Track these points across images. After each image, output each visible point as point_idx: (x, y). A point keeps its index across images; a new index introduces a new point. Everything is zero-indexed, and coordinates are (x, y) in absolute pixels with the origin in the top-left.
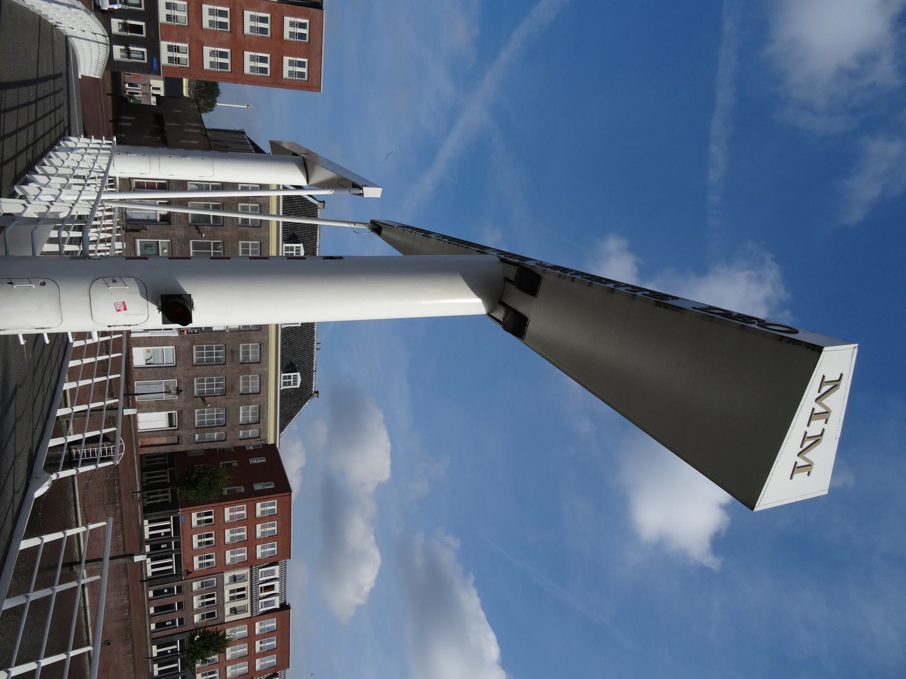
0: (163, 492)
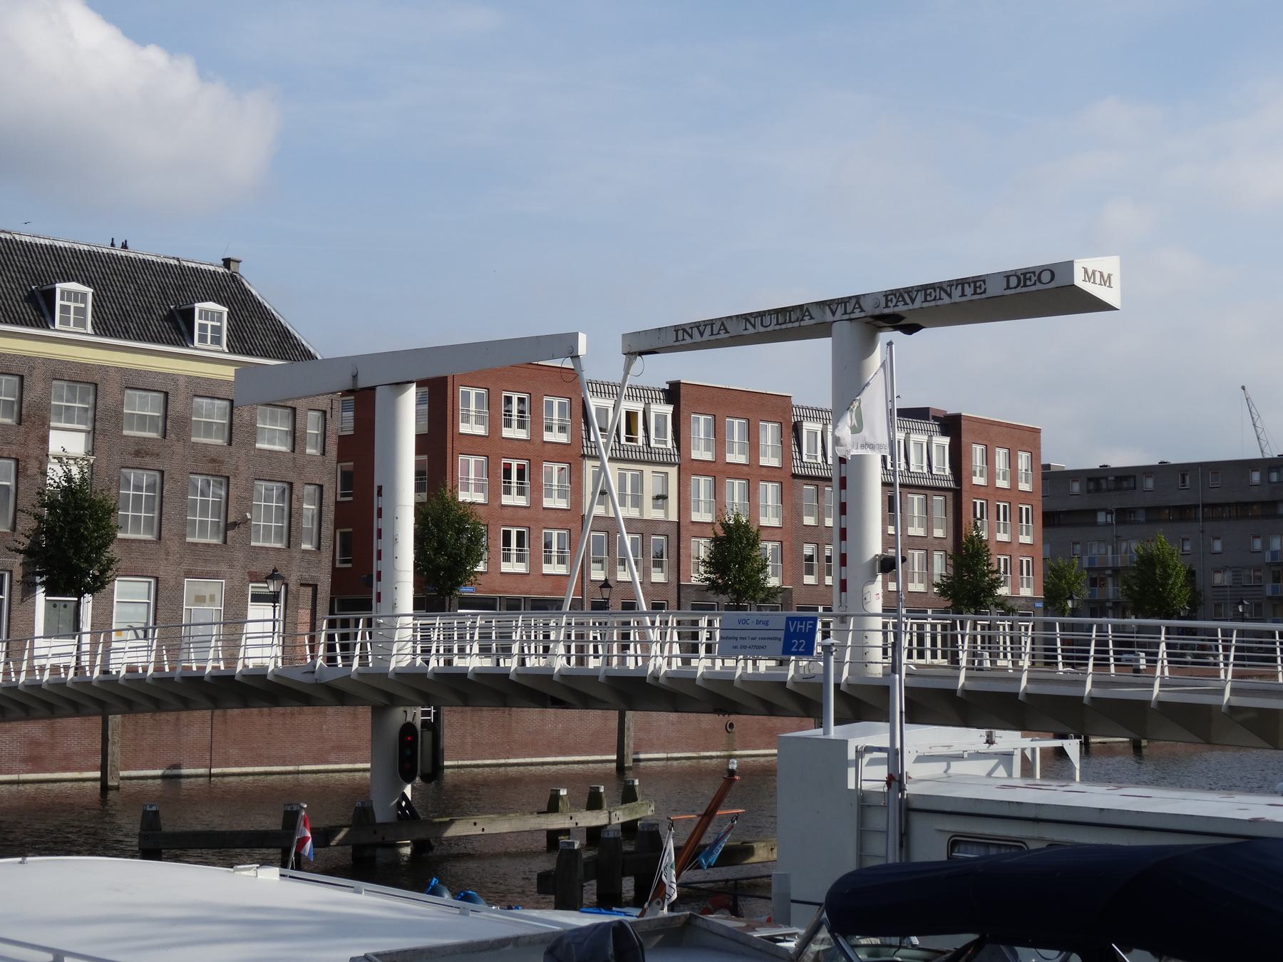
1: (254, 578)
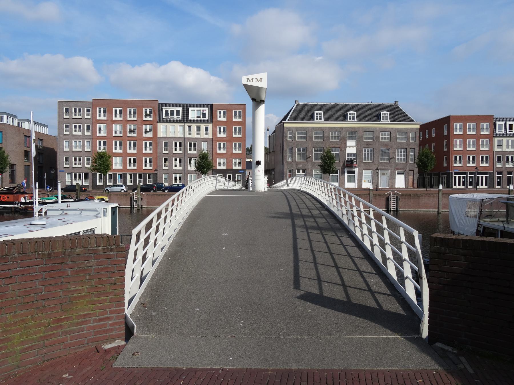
0: (442, 179)
1: (397, 169)
